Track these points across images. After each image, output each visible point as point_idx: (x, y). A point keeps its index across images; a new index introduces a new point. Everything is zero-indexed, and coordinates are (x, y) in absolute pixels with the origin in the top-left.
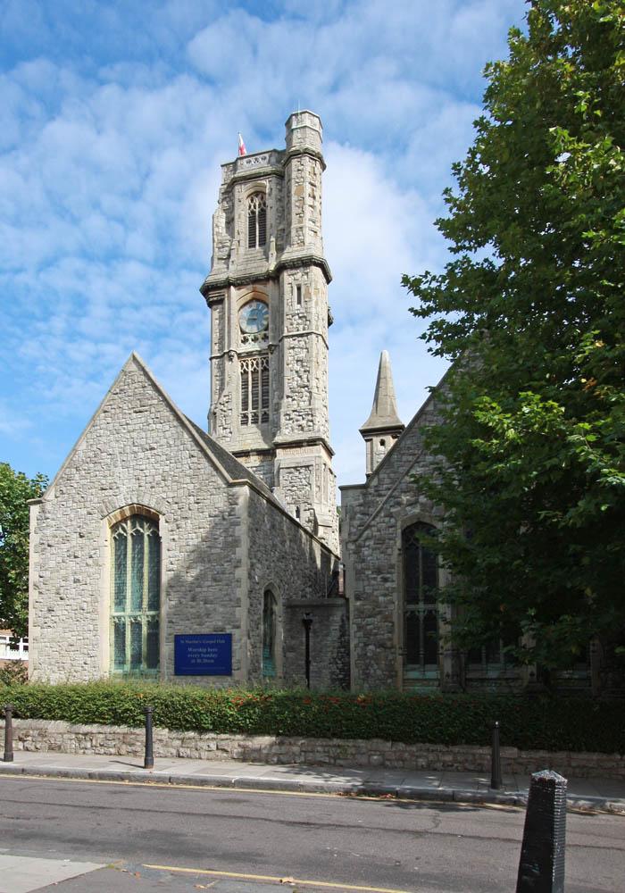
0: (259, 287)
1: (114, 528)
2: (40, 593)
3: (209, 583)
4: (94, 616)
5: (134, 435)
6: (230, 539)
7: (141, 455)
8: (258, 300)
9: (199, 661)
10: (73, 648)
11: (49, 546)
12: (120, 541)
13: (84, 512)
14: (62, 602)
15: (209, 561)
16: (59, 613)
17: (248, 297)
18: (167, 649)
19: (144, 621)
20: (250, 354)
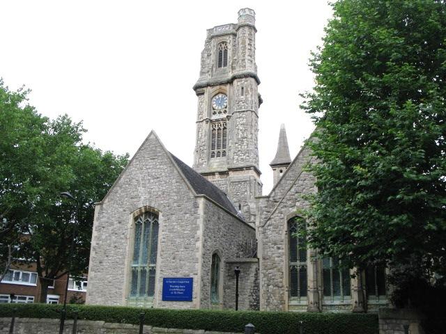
0: (223, 87)
1: (136, 219)
2: (96, 253)
3: (182, 250)
4: (122, 266)
5: (149, 170)
6: (194, 226)
7: (152, 181)
8: (222, 93)
9: (175, 293)
10: (111, 284)
11: (103, 227)
12: (138, 225)
13: (121, 210)
14: (106, 258)
15: (183, 238)
16: (104, 264)
17: (217, 92)
18: (159, 286)
19: (147, 269)
20: (217, 120)
